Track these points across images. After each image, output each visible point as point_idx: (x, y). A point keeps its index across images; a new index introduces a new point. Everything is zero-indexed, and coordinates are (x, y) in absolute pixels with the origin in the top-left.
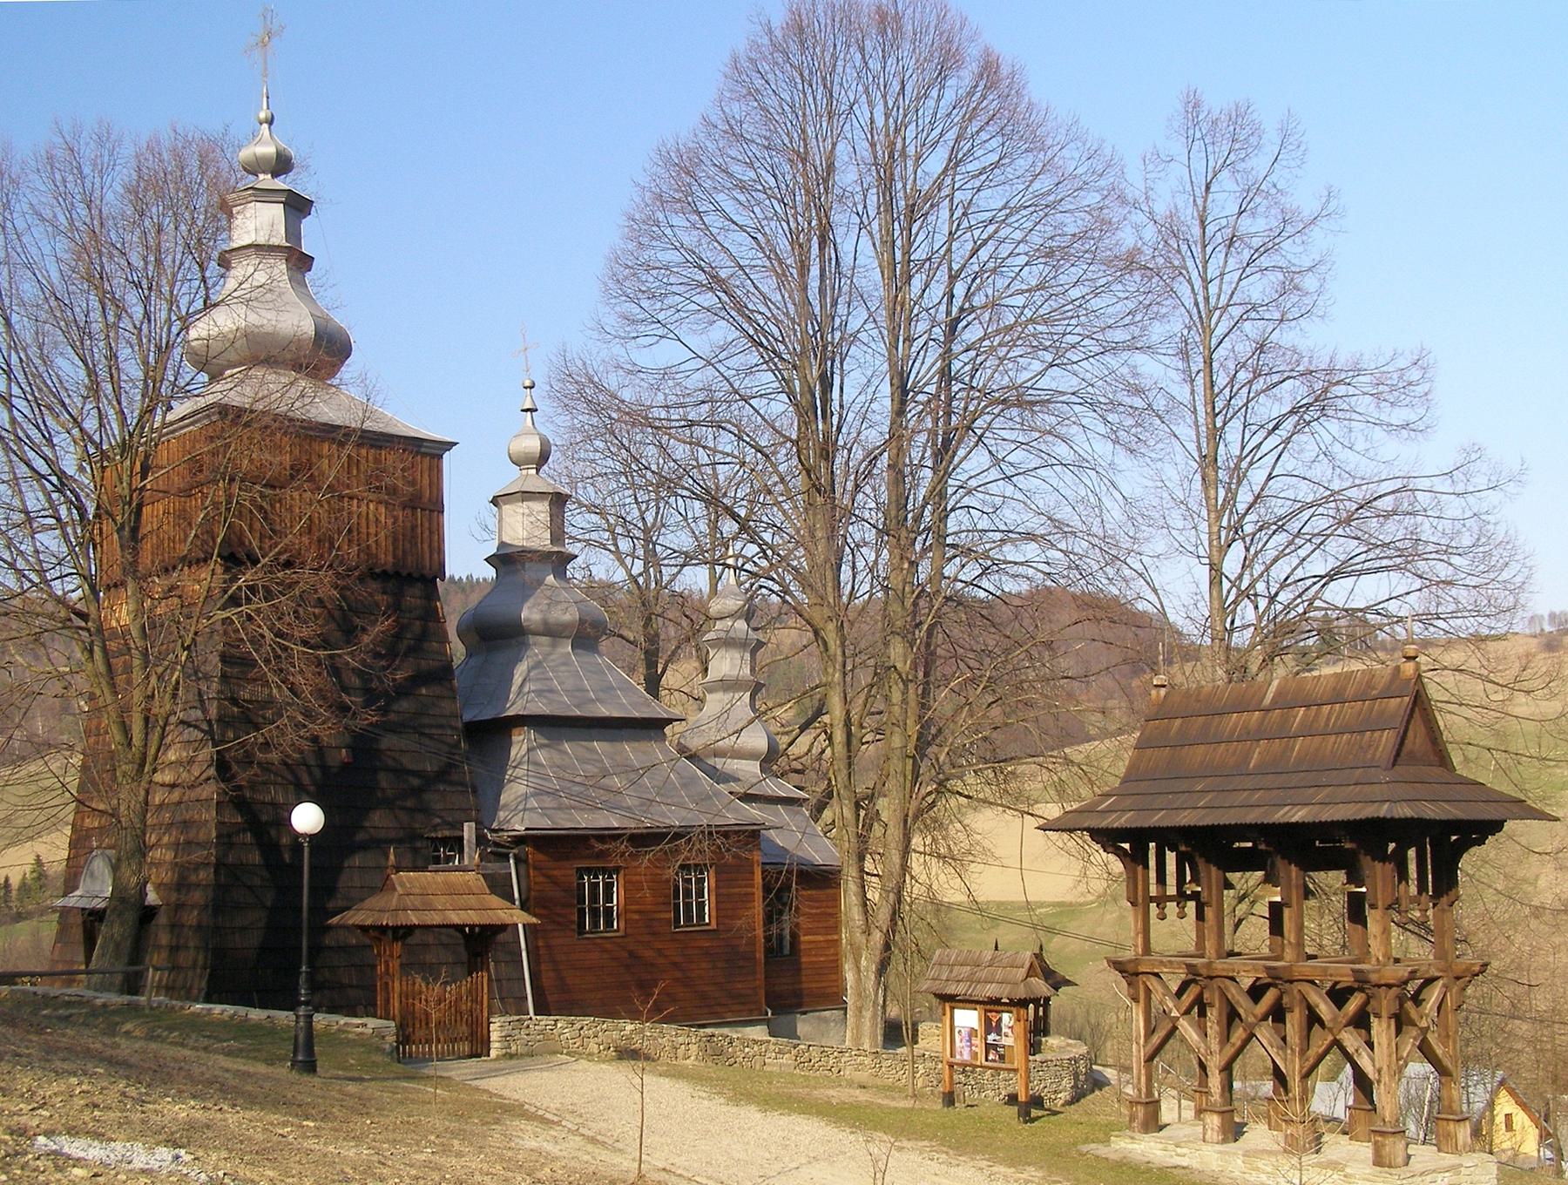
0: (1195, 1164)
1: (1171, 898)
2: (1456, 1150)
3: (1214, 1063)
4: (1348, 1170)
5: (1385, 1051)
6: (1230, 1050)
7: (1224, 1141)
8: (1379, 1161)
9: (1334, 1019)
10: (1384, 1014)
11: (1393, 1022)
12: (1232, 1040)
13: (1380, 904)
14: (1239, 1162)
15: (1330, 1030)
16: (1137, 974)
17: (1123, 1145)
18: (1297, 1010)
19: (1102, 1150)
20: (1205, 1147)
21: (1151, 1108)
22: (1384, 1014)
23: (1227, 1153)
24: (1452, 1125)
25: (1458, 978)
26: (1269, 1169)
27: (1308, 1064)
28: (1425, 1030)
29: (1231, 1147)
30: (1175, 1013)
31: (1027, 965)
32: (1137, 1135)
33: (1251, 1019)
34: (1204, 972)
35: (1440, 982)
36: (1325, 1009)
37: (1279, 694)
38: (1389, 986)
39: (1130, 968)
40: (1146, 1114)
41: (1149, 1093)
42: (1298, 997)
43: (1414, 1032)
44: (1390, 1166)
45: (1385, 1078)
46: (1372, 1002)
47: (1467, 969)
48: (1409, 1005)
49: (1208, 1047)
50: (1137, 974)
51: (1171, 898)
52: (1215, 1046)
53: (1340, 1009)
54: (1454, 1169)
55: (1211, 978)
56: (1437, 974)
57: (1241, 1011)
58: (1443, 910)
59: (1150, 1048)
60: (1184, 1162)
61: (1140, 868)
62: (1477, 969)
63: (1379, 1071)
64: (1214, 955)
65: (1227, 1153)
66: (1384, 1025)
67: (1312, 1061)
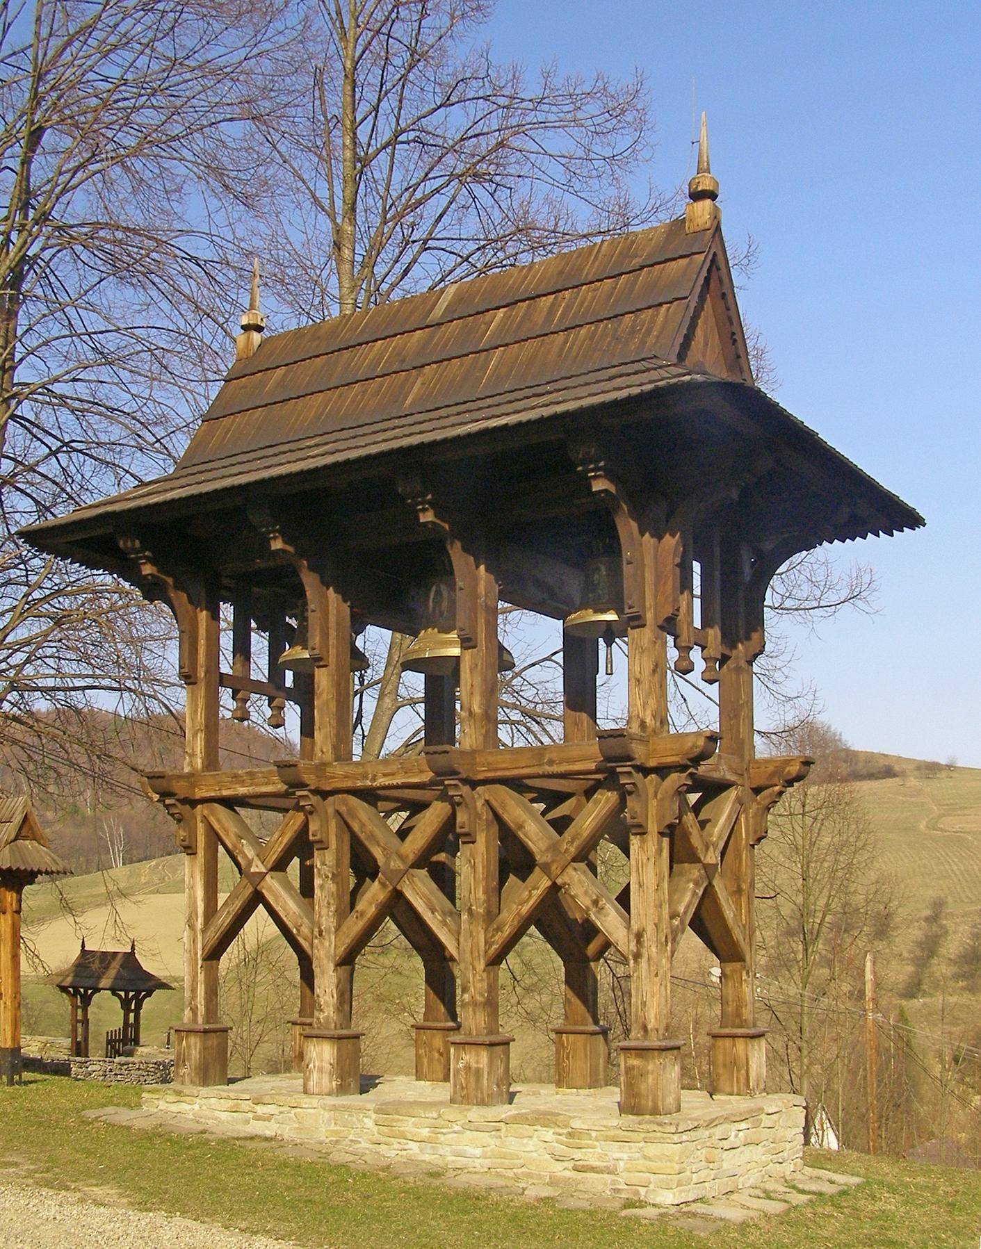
0: (287, 1132)
1: (257, 687)
2: (746, 1089)
3: (325, 954)
4: (576, 1124)
5: (652, 896)
6: (355, 926)
7: (342, 1090)
8: (631, 1106)
9: (554, 848)
10: (653, 827)
11: (666, 841)
12: (359, 907)
13: (649, 616)
14: (369, 1123)
15: (546, 868)
16: (193, 803)
17: (162, 1105)
18: (481, 839)
19: (123, 1116)
20: (305, 1101)
21: (213, 1040)
22: (653, 827)
23: (347, 1109)
24: (740, 1044)
25: (757, 791)
26: (425, 1132)
27: (500, 938)
28: (710, 870)
29: (355, 1099)
30: (258, 867)
31: (18, 818)
32: (188, 1089)
33: (396, 864)
34: (311, 780)
35: (732, 794)
36: (534, 831)
37: (459, 299)
38: (662, 771)
39: (180, 788)
40: (204, 1049)
41: (211, 1012)
42: (486, 815)
43: (695, 871)
44: (655, 1112)
45: (651, 947)
46: (631, 801)
47: (777, 772)
48: (689, 818)
49: (315, 923)
50: (193, 803)
51: (257, 687)
52: (327, 920)
53: (560, 833)
54: (752, 1115)
55: (325, 795)
56: (731, 777)
57: (377, 853)
58: (738, 670)
59: (214, 934)
60: (268, 1129)
61: (203, 616)
62: (794, 769)
63: (639, 936)
64: (329, 756)
65: (347, 1109)
66: (652, 848)
67: (508, 931)
